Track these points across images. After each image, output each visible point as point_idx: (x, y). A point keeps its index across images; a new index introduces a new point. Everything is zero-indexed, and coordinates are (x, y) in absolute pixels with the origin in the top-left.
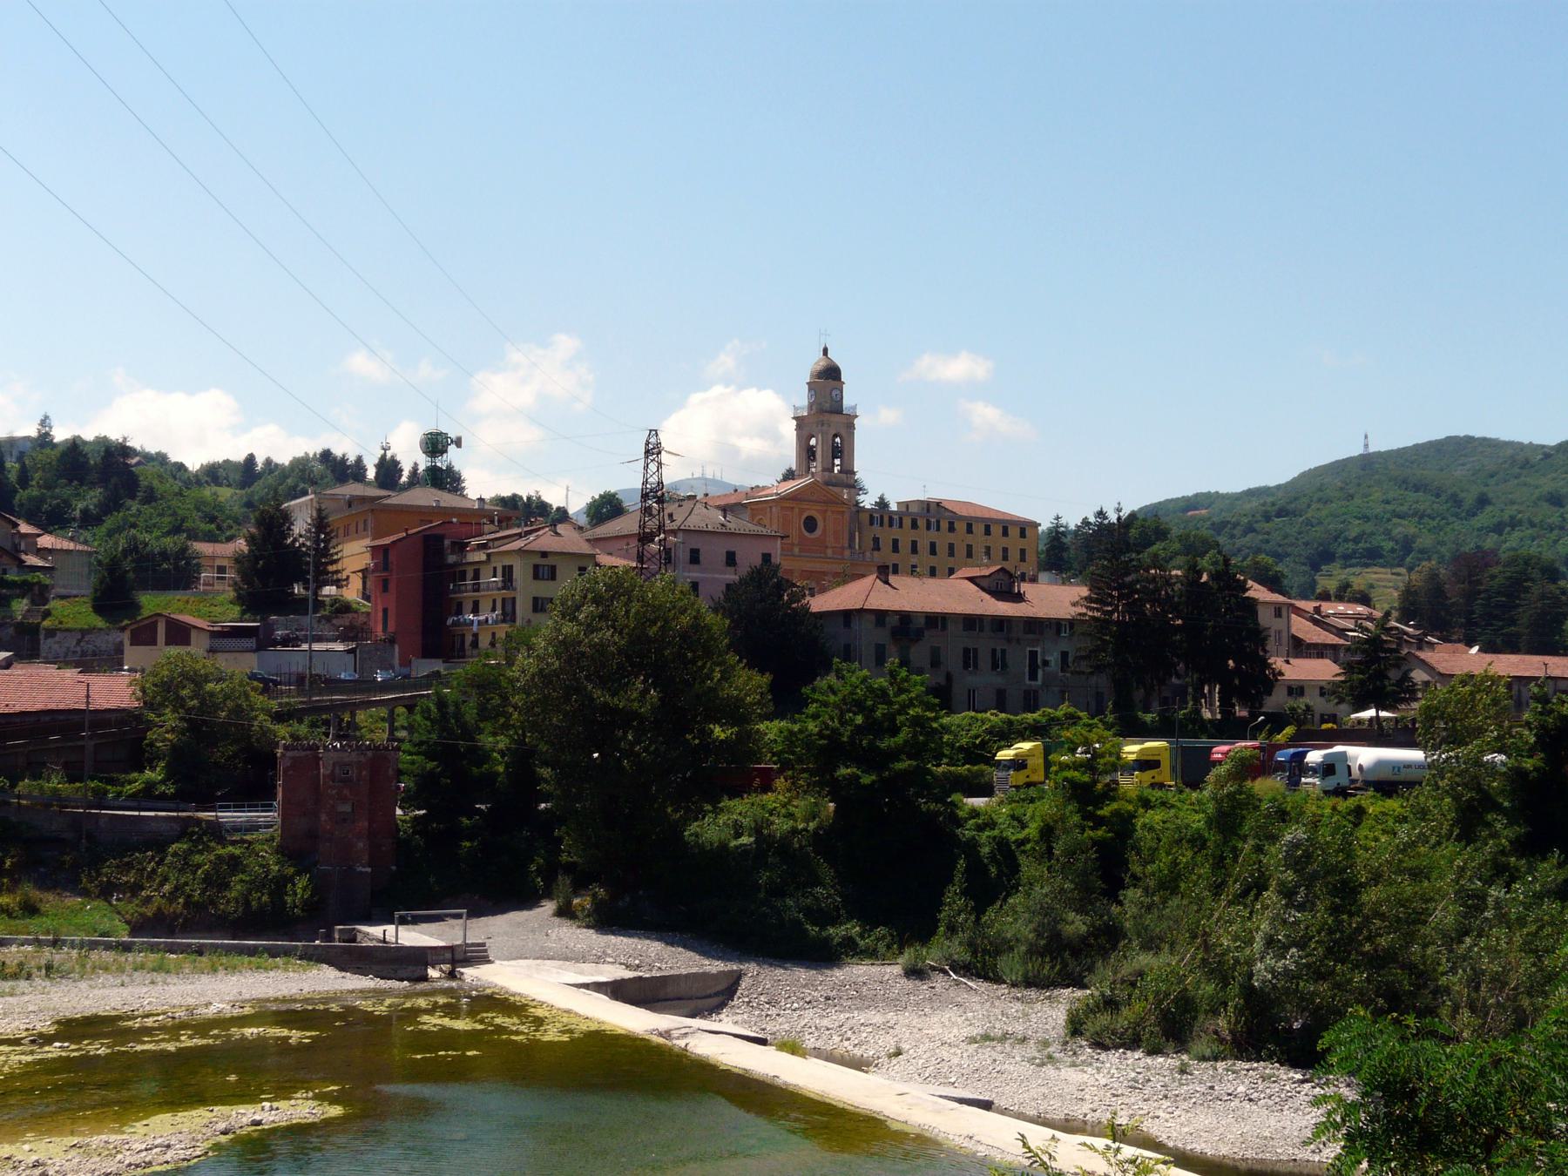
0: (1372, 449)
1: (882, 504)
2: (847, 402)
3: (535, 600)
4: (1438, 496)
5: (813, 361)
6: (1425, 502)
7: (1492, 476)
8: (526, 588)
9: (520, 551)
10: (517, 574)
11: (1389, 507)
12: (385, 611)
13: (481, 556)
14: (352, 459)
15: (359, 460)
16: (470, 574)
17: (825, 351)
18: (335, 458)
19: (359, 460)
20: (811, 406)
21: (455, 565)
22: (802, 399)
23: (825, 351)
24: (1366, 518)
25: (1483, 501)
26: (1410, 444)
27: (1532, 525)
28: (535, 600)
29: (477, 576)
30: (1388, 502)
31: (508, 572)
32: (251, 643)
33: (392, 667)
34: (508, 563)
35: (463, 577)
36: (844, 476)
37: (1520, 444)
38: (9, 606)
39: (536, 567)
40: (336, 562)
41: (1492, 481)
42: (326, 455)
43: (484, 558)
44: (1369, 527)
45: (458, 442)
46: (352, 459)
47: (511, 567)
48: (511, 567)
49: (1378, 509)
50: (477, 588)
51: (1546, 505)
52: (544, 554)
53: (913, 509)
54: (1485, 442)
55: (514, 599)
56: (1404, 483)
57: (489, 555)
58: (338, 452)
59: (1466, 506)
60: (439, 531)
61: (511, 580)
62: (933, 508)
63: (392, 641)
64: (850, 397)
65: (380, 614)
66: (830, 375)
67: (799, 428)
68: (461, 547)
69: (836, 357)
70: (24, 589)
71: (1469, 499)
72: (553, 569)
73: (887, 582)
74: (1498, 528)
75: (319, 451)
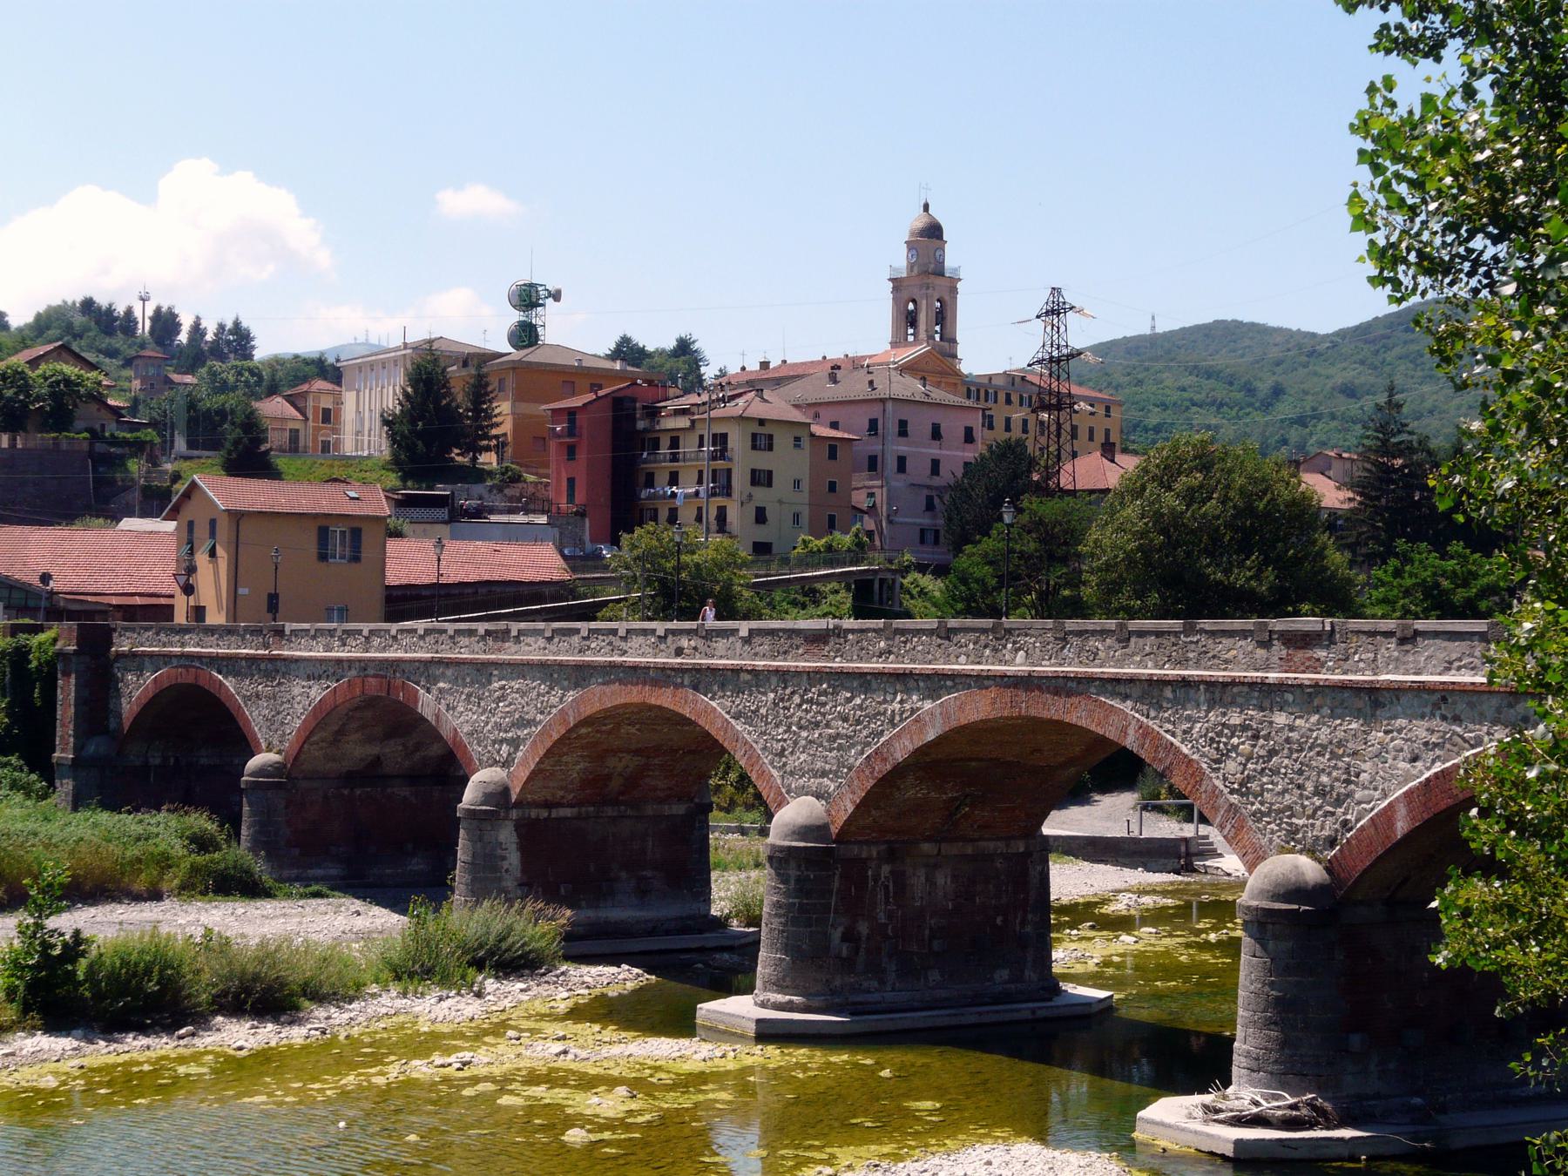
0: (1159, 330)
1: (723, 373)
2: (950, 262)
3: (753, 471)
4: (1231, 384)
5: (916, 220)
6: (1221, 393)
7: (1278, 364)
8: (742, 459)
9: (741, 419)
10: (733, 442)
11: (1185, 395)
12: (571, 481)
13: (683, 422)
14: (120, 310)
15: (129, 312)
16: (665, 442)
17: (926, 208)
18: (99, 308)
19: (129, 312)
20: (911, 267)
21: (645, 430)
22: (899, 260)
23: (926, 208)
24: (1164, 406)
25: (1278, 392)
26: (1176, 327)
27: (1333, 417)
28: (753, 471)
29: (675, 443)
30: (1184, 390)
31: (721, 440)
32: (443, 513)
33: (582, 542)
34: (723, 431)
35: (656, 444)
36: (946, 344)
37: (1314, 335)
38: (124, 465)
39: (754, 436)
40: (498, 425)
41: (1279, 370)
42: (88, 305)
43: (688, 424)
44: (1168, 416)
45: (556, 296)
46: (120, 310)
47: (724, 436)
48: (724, 436)
49: (1176, 396)
50: (674, 458)
51: (1342, 398)
52: (762, 422)
53: (1000, 382)
54: (1253, 326)
55: (729, 471)
56: (1195, 370)
57: (693, 422)
58: (102, 301)
59: (1261, 395)
60: (628, 393)
61: (724, 449)
62: (1017, 380)
63: (581, 514)
64: (952, 259)
65: (565, 483)
66: (933, 231)
67: (896, 289)
68: (653, 413)
69: (936, 213)
70: (138, 447)
71: (1264, 387)
72: (771, 437)
73: (1113, 461)
74: (1301, 421)
75: (79, 299)
